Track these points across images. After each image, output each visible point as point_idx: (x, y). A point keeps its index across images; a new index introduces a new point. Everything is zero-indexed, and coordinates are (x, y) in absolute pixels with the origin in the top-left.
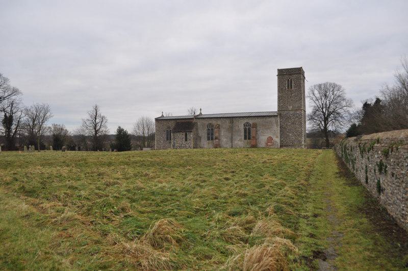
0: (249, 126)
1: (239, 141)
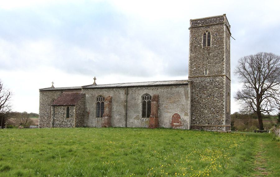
0: (150, 101)
1: (136, 119)
